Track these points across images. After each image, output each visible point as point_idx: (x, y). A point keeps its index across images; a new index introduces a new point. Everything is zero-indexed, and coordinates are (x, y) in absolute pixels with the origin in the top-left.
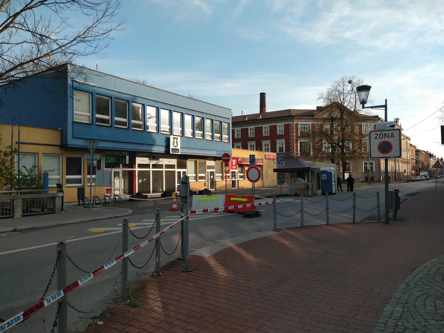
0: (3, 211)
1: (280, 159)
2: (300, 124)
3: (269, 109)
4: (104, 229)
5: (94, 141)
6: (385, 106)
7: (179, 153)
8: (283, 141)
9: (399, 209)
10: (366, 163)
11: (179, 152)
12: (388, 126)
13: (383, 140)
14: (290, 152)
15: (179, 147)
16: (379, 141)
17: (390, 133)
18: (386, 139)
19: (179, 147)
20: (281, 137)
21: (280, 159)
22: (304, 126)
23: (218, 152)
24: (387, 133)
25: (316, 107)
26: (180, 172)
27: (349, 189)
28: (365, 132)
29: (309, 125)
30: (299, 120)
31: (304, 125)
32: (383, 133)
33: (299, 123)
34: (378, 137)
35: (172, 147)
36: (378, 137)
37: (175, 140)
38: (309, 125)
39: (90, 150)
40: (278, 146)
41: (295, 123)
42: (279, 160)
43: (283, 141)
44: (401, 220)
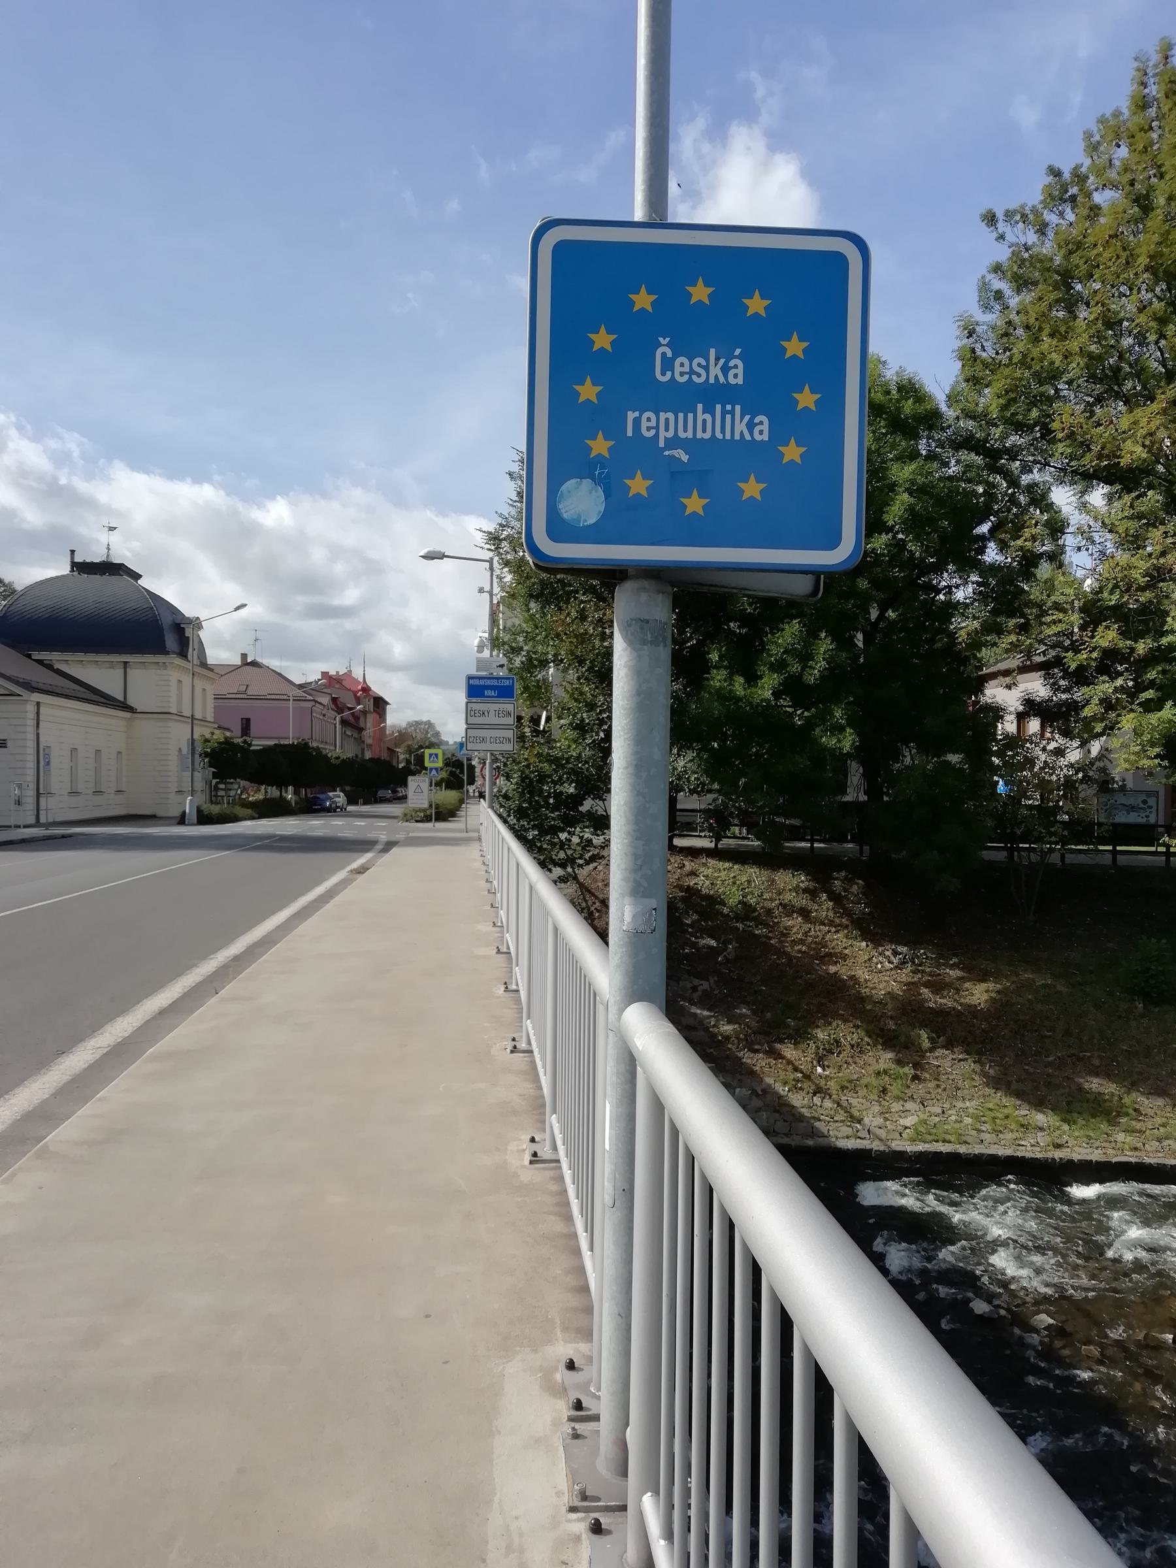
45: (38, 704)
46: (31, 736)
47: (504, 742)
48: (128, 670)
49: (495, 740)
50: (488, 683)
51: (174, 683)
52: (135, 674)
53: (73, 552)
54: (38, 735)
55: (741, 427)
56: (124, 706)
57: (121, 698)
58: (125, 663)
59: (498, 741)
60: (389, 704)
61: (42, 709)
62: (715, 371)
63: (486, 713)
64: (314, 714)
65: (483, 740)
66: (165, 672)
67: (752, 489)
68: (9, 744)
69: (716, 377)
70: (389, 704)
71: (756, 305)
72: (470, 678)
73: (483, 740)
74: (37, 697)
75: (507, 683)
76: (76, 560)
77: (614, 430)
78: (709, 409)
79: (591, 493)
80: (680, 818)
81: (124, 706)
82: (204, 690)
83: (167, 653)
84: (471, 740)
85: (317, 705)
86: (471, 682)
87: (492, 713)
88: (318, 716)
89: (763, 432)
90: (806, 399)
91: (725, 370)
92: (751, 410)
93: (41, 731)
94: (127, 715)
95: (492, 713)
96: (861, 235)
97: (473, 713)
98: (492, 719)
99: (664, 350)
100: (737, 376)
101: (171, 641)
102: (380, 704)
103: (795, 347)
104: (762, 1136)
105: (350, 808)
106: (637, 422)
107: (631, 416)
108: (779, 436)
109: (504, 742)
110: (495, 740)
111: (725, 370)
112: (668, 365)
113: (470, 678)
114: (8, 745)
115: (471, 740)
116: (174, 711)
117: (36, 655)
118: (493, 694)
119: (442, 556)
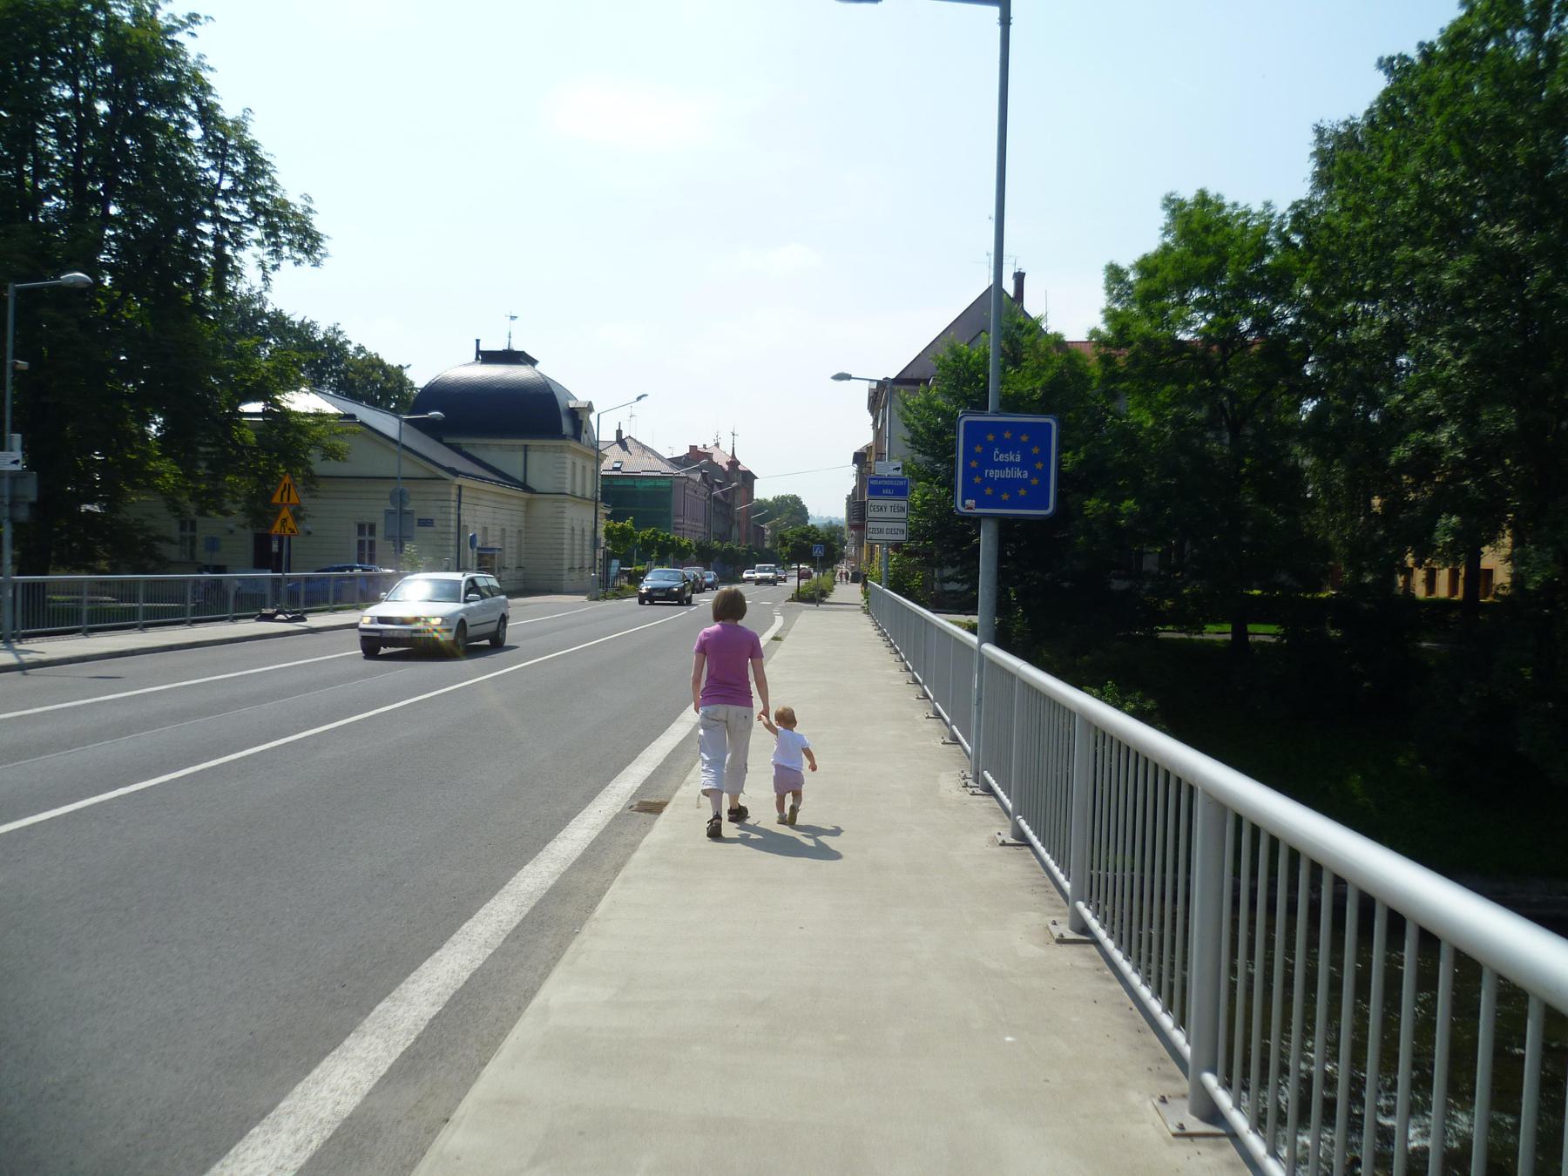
45: (460, 487)
46: (454, 517)
48: (528, 453)
49: (890, 531)
50: (886, 483)
51: (569, 466)
52: (534, 457)
53: (478, 341)
54: (459, 515)
55: (1019, 474)
56: (526, 488)
57: (520, 477)
58: (526, 446)
60: (757, 478)
61: (463, 492)
62: (1012, 457)
64: (687, 491)
65: (881, 531)
66: (562, 455)
67: (1022, 492)
68: (436, 522)
70: (757, 478)
71: (1024, 438)
73: (881, 531)
74: (459, 481)
75: (901, 483)
76: (481, 349)
77: (982, 475)
78: (1010, 469)
81: (526, 488)
82: (574, 463)
83: (564, 437)
84: (871, 531)
85: (691, 483)
87: (889, 509)
88: (690, 493)
89: (1026, 475)
90: (1039, 466)
91: (1015, 458)
92: (1022, 469)
93: (462, 512)
94: (526, 495)
95: (889, 509)
98: (888, 514)
99: (996, 452)
100: (1018, 459)
101: (567, 427)
102: (749, 478)
103: (1035, 450)
104: (1238, 1133)
106: (988, 473)
107: (987, 471)
108: (1030, 477)
110: (890, 531)
111: (1015, 458)
112: (997, 456)
114: (435, 524)
115: (871, 531)
116: (568, 491)
117: (447, 440)
119: (848, 377)
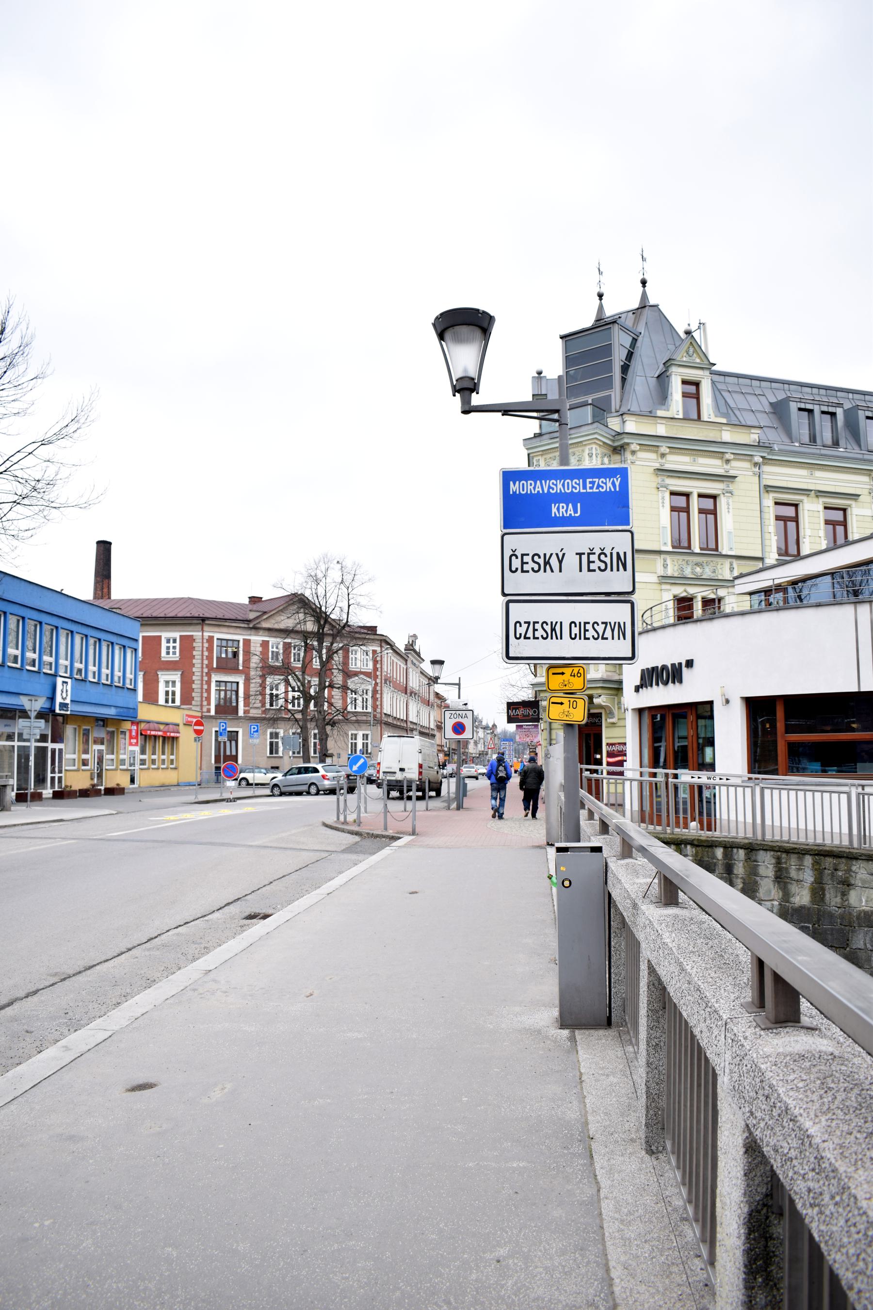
0: (103, 792)
1: (254, 728)
2: (218, 639)
3: (120, 590)
4: (172, 818)
5: (36, 698)
6: (459, 685)
7: (69, 713)
8: (176, 677)
9: (466, 796)
10: (367, 735)
11: (67, 711)
12: (461, 704)
13: (458, 720)
14: (191, 704)
15: (68, 701)
16: (454, 721)
17: (464, 713)
18: (460, 720)
19: (68, 701)
20: (170, 666)
21: (254, 728)
22: (227, 643)
23: (119, 710)
24: (460, 712)
25: (249, 598)
26: (55, 749)
27: (592, 747)
28: (354, 667)
29: (239, 641)
30: (216, 629)
31: (227, 640)
32: (458, 712)
33: (217, 636)
34: (452, 717)
35: (59, 700)
36: (452, 717)
37: (65, 685)
38: (239, 641)
39: (29, 712)
40: (162, 689)
41: (206, 634)
42: (252, 730)
43: (176, 677)
44: (467, 809)
47: (608, 633)
50: (559, 487)
59: (591, 633)
63: (554, 562)
65: (553, 631)
69: (610, 488)
72: (509, 477)
73: (553, 631)
75: (608, 485)
79: (454, 395)
80: (832, 545)
84: (521, 630)
86: (514, 487)
87: (571, 561)
95: (571, 561)
96: (482, 308)
97: (516, 563)
105: (183, 707)
109: (608, 633)
113: (509, 477)
115: (521, 630)
118: (571, 512)
